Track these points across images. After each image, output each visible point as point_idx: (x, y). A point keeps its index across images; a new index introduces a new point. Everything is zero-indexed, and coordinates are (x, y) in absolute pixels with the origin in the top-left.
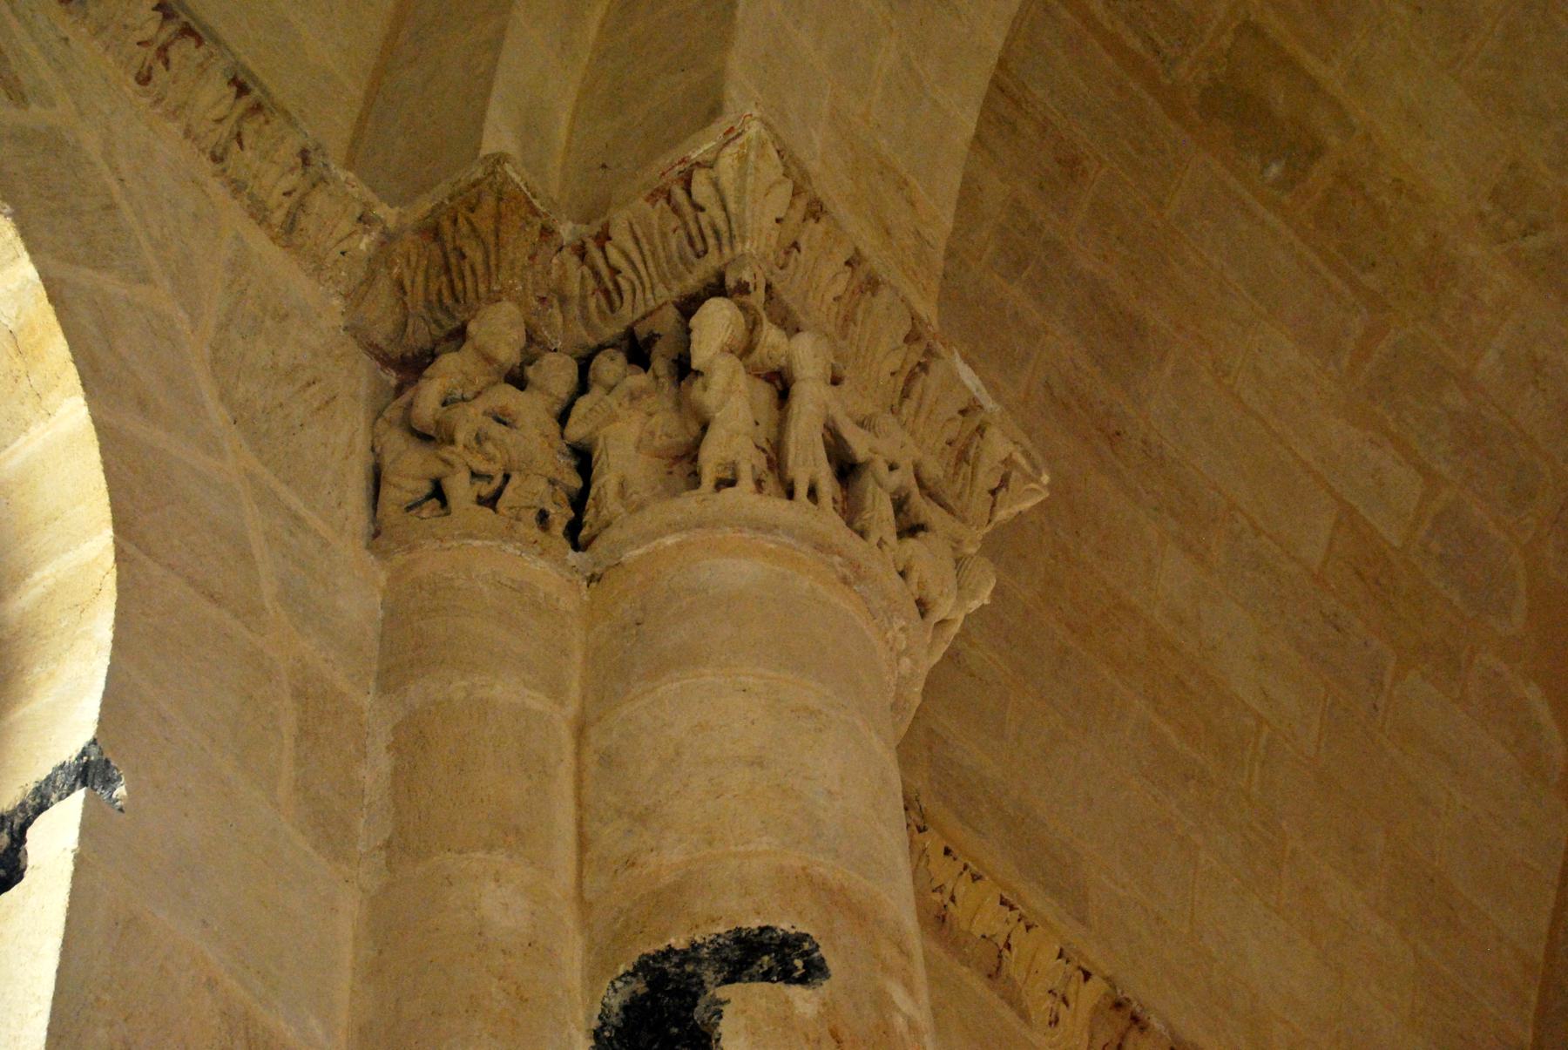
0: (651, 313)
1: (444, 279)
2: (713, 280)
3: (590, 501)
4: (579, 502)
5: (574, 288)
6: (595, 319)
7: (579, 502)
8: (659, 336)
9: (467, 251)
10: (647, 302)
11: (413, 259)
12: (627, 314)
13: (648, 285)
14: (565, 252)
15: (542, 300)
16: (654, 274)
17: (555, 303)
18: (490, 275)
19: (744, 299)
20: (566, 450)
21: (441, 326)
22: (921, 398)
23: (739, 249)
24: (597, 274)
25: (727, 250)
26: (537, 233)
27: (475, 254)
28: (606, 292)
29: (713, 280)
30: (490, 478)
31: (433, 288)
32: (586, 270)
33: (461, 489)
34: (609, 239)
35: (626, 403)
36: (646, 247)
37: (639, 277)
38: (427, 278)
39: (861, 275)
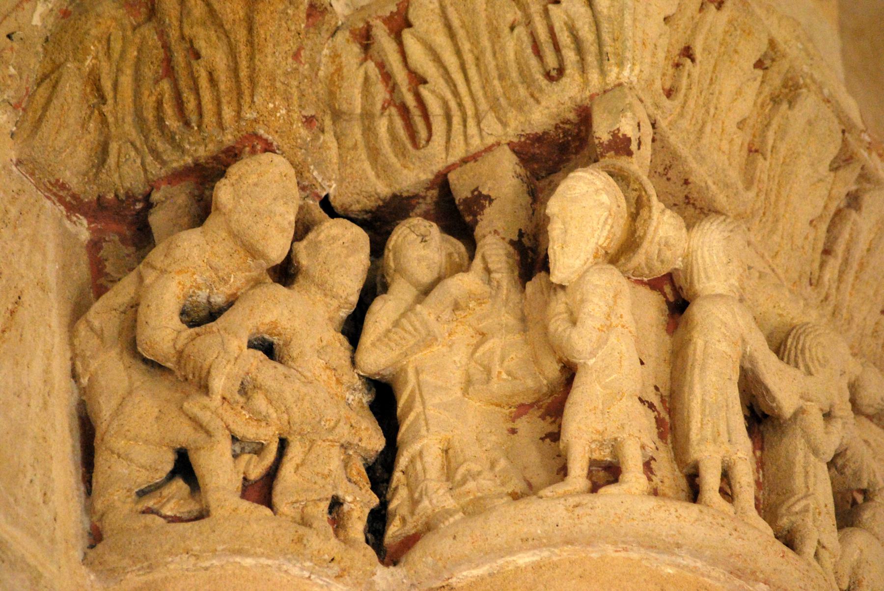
0: (475, 157)
1: (165, 85)
2: (572, 116)
3: (397, 475)
4: (381, 471)
5: (353, 98)
6: (386, 148)
7: (381, 471)
8: (490, 199)
9: (201, 45)
10: (478, 143)
11: (117, 46)
12: (437, 156)
13: (470, 112)
14: (341, 37)
15: (309, 121)
16: (480, 94)
17: (328, 122)
18: (240, 95)
19: (622, 162)
20: (358, 383)
21: (163, 163)
22: (848, 250)
23: (613, 73)
24: (387, 77)
25: (594, 76)
26: (303, 15)
27: (216, 56)
28: (404, 110)
29: (572, 116)
30: (259, 449)
31: (149, 102)
32: (371, 65)
33: (221, 471)
34: (409, 25)
35: (447, 315)
36: (466, 46)
37: (456, 93)
38: (138, 79)
39: (776, 81)
